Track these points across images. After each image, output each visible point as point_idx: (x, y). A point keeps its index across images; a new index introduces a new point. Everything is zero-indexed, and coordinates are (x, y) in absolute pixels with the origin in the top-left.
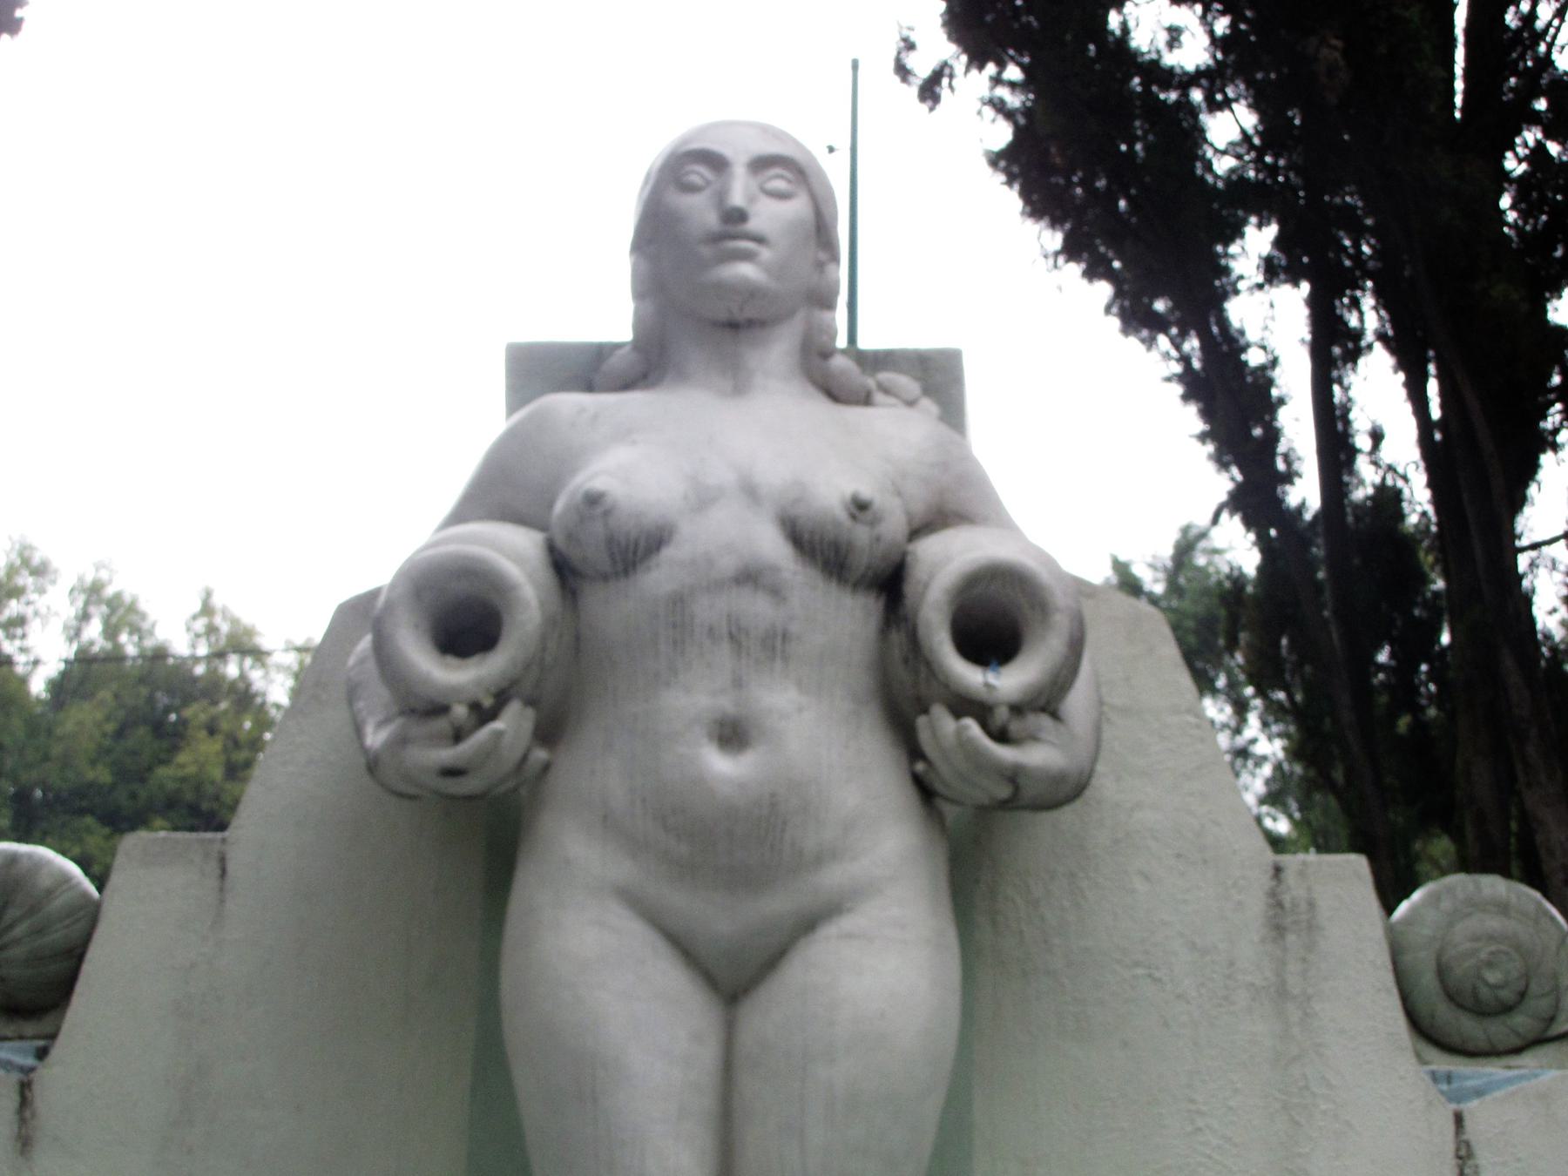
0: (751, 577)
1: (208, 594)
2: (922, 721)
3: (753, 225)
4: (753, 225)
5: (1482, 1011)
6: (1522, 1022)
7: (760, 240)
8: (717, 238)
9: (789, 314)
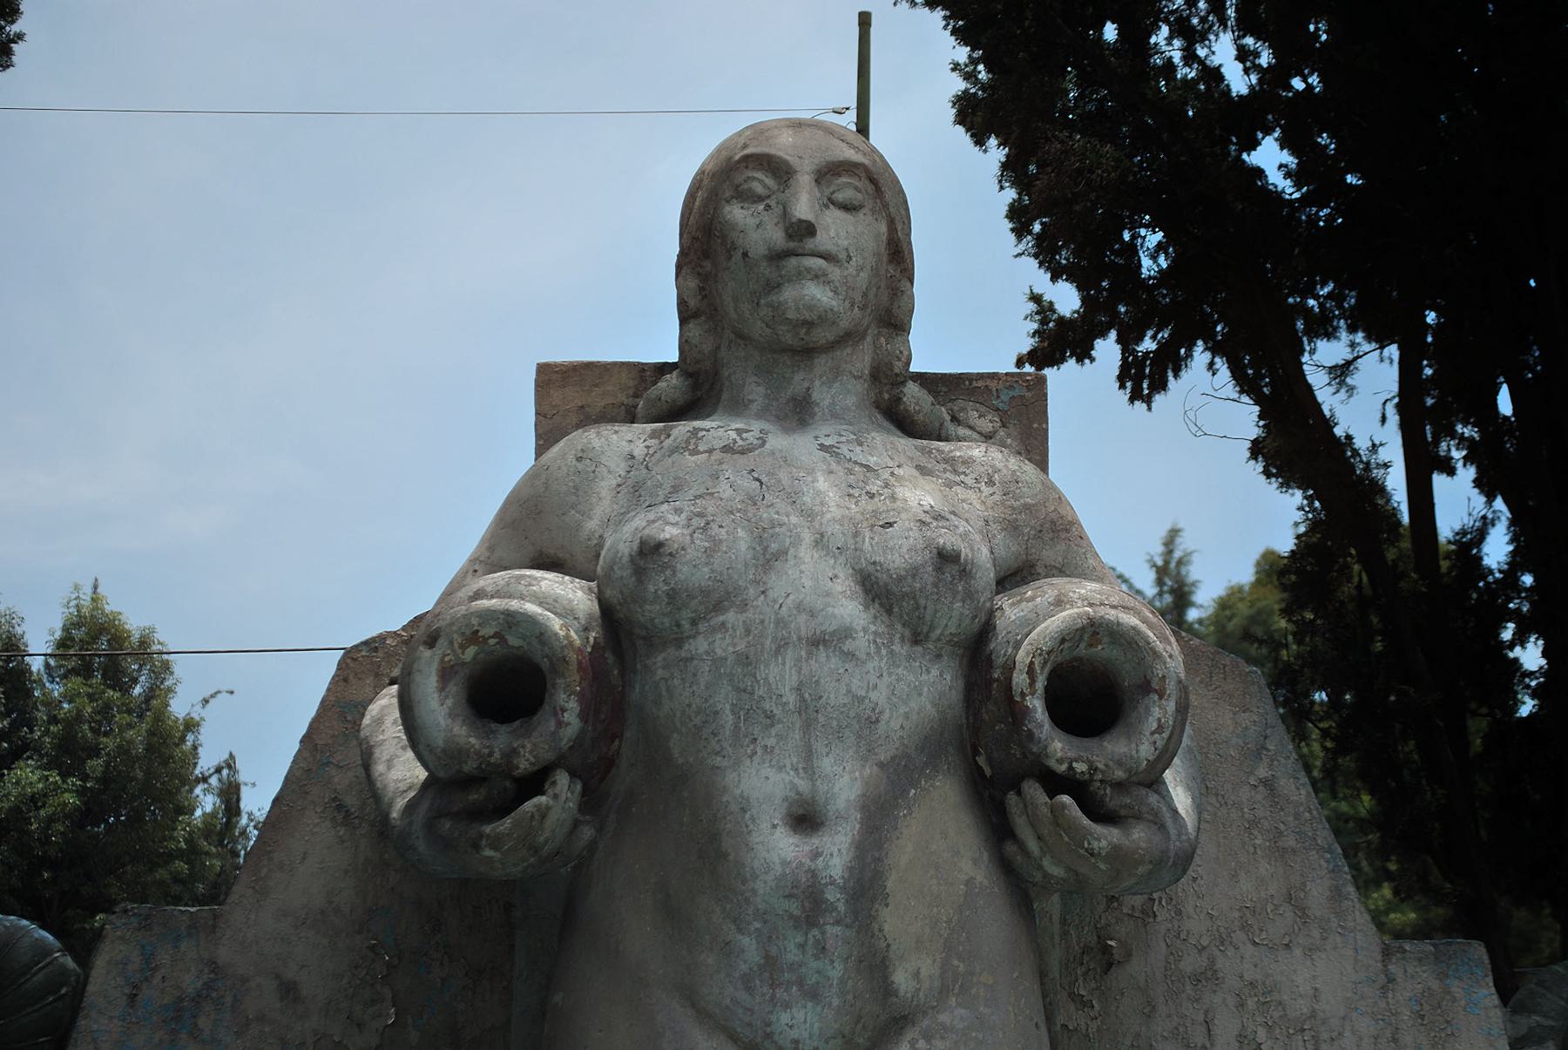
0: (880, 604)
1: (1150, 409)
2: (1012, 798)
3: (822, 240)
4: (822, 240)
7: (827, 256)
8: (777, 256)
9: (849, 338)
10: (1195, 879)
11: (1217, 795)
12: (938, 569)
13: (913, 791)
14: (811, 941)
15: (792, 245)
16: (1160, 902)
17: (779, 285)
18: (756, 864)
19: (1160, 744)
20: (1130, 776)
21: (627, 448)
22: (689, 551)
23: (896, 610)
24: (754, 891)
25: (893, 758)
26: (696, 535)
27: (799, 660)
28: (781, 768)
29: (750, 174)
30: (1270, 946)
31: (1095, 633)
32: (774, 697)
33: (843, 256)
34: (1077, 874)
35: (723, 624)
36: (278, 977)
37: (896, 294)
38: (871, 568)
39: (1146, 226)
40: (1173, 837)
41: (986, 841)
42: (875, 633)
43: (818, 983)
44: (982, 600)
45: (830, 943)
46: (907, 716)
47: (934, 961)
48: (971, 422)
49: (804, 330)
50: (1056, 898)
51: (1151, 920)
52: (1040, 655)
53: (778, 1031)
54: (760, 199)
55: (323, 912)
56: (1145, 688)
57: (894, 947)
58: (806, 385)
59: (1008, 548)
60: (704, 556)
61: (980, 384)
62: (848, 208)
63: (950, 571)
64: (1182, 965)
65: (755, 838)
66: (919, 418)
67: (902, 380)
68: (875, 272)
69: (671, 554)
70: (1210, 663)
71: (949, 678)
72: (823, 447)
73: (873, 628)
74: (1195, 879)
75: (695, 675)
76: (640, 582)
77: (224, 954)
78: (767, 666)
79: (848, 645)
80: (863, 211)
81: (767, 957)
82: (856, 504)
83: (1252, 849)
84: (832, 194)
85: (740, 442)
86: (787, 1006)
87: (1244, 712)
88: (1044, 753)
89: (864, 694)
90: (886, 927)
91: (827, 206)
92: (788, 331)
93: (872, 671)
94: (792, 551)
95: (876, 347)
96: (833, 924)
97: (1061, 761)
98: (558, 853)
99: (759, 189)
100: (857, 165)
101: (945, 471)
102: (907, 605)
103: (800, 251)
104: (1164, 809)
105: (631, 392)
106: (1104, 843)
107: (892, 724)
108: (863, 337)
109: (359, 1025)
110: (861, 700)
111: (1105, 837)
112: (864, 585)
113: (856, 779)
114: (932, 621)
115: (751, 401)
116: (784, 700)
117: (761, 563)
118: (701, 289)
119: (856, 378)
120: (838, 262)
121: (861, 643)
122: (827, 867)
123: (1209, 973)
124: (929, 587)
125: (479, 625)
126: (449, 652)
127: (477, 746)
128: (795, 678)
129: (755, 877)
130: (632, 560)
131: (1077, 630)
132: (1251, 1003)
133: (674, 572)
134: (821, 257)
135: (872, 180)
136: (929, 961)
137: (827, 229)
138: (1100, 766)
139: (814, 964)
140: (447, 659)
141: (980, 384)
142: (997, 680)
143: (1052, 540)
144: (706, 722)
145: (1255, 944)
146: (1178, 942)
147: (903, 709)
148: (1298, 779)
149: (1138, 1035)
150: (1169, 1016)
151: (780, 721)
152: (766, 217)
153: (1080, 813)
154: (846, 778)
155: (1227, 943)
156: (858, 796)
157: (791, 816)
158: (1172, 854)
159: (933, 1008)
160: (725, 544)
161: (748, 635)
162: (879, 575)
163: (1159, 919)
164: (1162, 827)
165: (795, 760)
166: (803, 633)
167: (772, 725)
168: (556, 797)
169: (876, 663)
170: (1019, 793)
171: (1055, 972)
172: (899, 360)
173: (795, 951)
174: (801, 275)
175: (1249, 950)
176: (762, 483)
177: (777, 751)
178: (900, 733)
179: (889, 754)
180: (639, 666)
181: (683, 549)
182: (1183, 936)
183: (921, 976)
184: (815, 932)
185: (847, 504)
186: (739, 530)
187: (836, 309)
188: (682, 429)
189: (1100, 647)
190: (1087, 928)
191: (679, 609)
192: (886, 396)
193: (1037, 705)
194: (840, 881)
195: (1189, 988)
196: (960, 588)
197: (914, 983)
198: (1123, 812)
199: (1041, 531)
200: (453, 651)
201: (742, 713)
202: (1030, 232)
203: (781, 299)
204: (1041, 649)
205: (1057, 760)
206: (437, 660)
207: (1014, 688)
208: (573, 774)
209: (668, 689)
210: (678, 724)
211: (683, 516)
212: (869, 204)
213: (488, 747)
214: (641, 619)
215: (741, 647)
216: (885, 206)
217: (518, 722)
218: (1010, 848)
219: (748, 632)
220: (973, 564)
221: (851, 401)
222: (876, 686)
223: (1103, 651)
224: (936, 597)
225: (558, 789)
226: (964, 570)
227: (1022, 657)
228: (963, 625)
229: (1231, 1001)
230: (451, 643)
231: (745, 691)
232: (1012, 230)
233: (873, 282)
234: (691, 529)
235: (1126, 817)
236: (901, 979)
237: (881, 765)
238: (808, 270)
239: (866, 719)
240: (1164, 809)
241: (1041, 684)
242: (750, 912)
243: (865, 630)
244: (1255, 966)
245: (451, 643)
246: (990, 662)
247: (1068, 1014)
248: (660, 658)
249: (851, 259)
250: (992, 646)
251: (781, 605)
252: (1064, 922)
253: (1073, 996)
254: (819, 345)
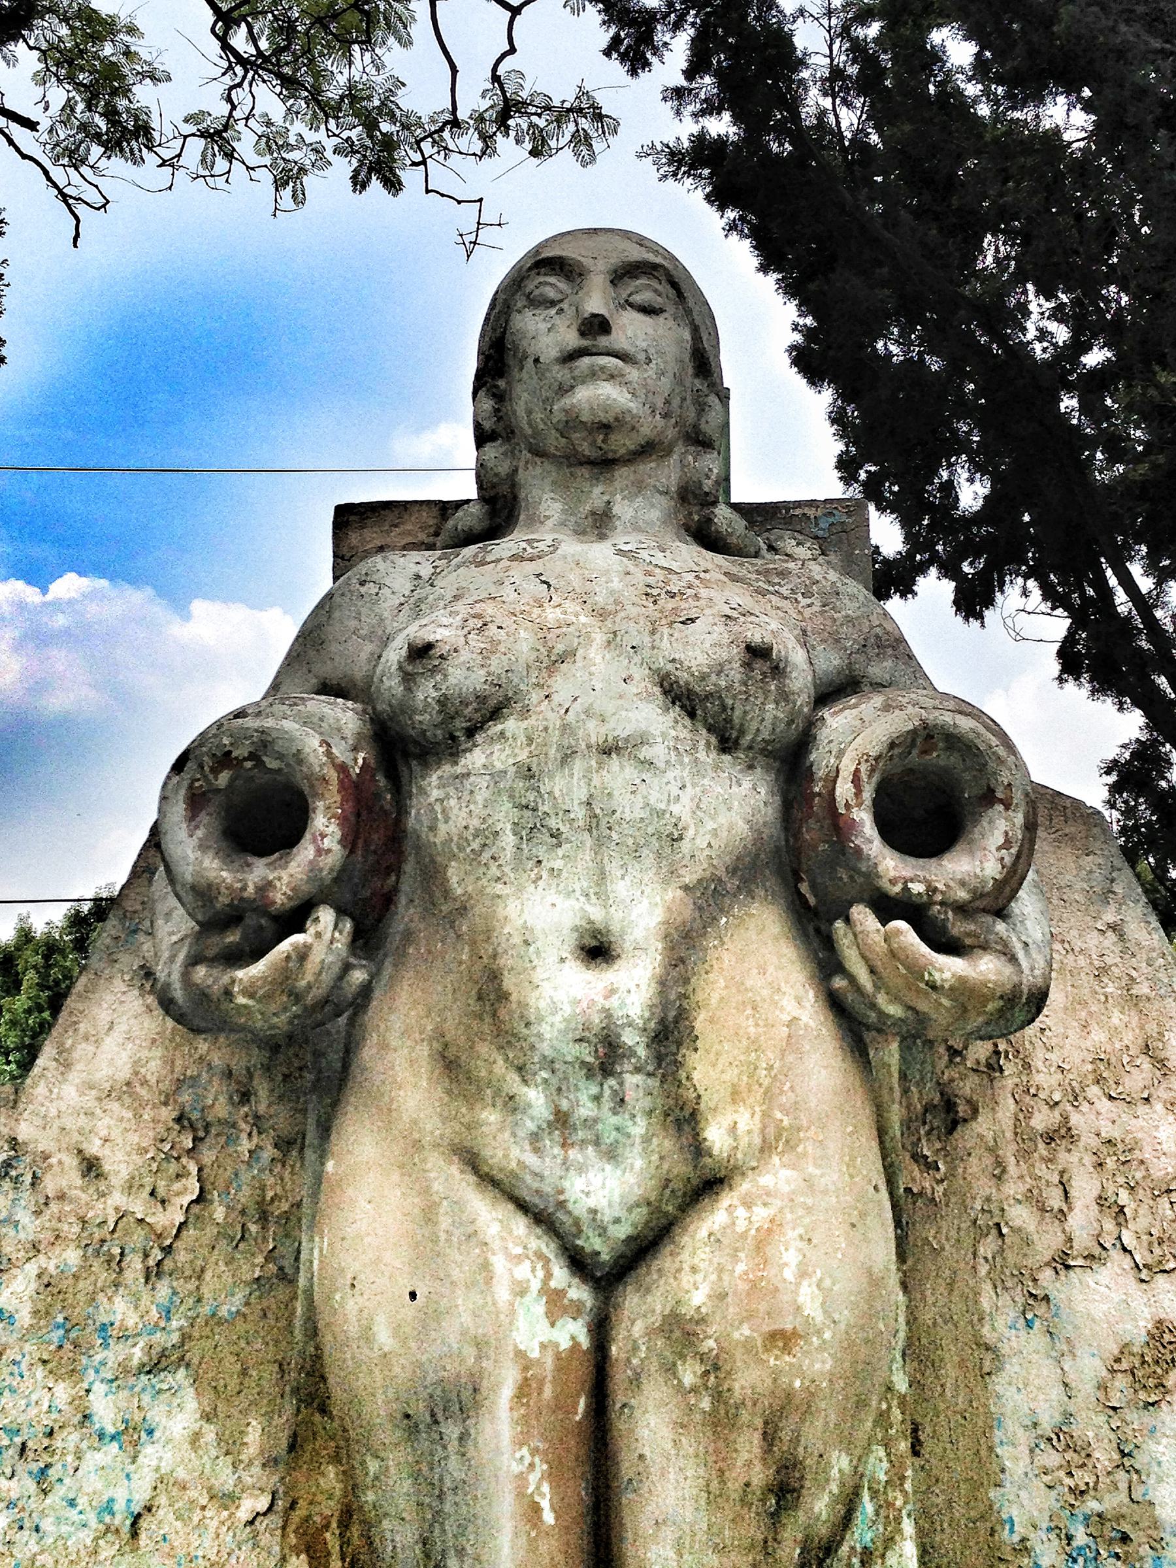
0: (682, 707)
7: (623, 357)
10: (1042, 1030)
11: (1063, 942)
12: (747, 665)
13: (724, 920)
14: (607, 1092)
15: (585, 343)
16: (1007, 1057)
17: (572, 387)
18: (542, 1004)
19: (1008, 860)
20: (974, 899)
21: (415, 569)
22: (462, 652)
23: (699, 712)
24: (539, 1036)
25: (700, 881)
26: (470, 636)
27: (589, 770)
28: (570, 893)
29: (542, 279)
30: (1128, 1100)
31: (930, 737)
32: (561, 813)
33: (641, 357)
34: (917, 1012)
35: (502, 733)
36: (80, 1152)
37: (703, 410)
38: (670, 667)
40: (1027, 971)
41: (794, 938)
42: (677, 738)
43: (617, 1142)
44: (799, 703)
45: (630, 1096)
46: (715, 833)
47: (753, 1115)
48: (789, 551)
49: (601, 437)
50: (894, 1046)
51: (997, 1074)
52: (867, 761)
53: (572, 1200)
54: (553, 303)
55: (128, 1084)
57: (704, 1099)
58: (606, 498)
59: (830, 661)
60: (480, 657)
61: (797, 512)
62: (648, 310)
63: (759, 666)
64: (1033, 1123)
65: (538, 975)
66: (733, 540)
67: (713, 499)
68: (678, 380)
69: (441, 657)
70: (1049, 806)
71: (763, 792)
72: (620, 552)
73: (673, 733)
74: (1042, 1030)
75: (472, 792)
76: (409, 689)
77: (24, 1131)
78: (551, 777)
79: (645, 753)
80: (665, 315)
82: (655, 603)
83: (1103, 998)
84: (629, 296)
85: (529, 550)
86: (581, 1169)
87: (1087, 855)
88: (872, 875)
89: (663, 806)
90: (696, 1076)
91: (623, 307)
92: (584, 439)
93: (673, 782)
94: (580, 653)
95: (683, 465)
96: (632, 1073)
97: (893, 882)
98: (327, 1002)
99: (551, 293)
100: (656, 267)
101: (757, 580)
102: (712, 707)
103: (594, 350)
104: (1014, 939)
105: (432, 530)
106: (947, 975)
107: (698, 841)
108: (669, 453)
109: (163, 1202)
110: (660, 814)
111: (948, 968)
112: (662, 686)
113: (656, 904)
114: (742, 725)
115: (547, 517)
116: (572, 816)
117: (544, 665)
118: (497, 410)
119: (661, 493)
120: (636, 363)
121: (657, 752)
122: (623, 1004)
123: (1063, 1131)
124: (736, 685)
125: (232, 744)
126: (198, 776)
127: (228, 881)
128: (585, 791)
129: (541, 1019)
130: (400, 668)
131: (908, 732)
132: (1110, 1163)
133: (446, 676)
134: (616, 356)
135: (674, 285)
136: (747, 1115)
137: (623, 328)
138: (941, 886)
139: (614, 1120)
140: (197, 784)
141: (797, 512)
142: (819, 794)
143: (878, 655)
144: (485, 845)
145: (1111, 1098)
146: (1028, 1098)
147: (710, 825)
148: (1149, 923)
149: (988, 1199)
150: (1021, 1177)
151: (568, 841)
152: (557, 320)
153: (918, 940)
154: (646, 902)
155: (1080, 1099)
156: (659, 923)
157: (582, 949)
158: (1026, 991)
159: (753, 1169)
160: (503, 645)
161: (529, 745)
162: (678, 673)
163: (1006, 1073)
164: (1013, 959)
165: (585, 884)
166: (593, 740)
167: (559, 845)
168: (318, 935)
169: (677, 772)
170: (847, 920)
171: (896, 1129)
172: (708, 478)
173: (590, 1105)
174: (594, 375)
175: (1104, 1105)
176: (549, 586)
177: (565, 874)
178: (707, 852)
179: (695, 877)
180: (414, 790)
181: (456, 651)
182: (1032, 1091)
183: (739, 1132)
184: (612, 1082)
185: (645, 603)
186: (522, 631)
187: (635, 411)
189: (935, 754)
190: (929, 1085)
191: (452, 718)
192: (696, 518)
193: (864, 818)
194: (640, 1023)
195: (1041, 1146)
196: (773, 687)
197: (731, 1141)
198: (968, 941)
199: (864, 646)
200: (205, 777)
201: (524, 833)
202: (857, 481)
203: (575, 401)
204: (867, 754)
205: (890, 881)
206: (186, 784)
207: (838, 799)
208: (341, 912)
209: (443, 811)
210: (456, 850)
211: (458, 618)
212: (671, 309)
213: (241, 881)
214: (412, 733)
215: (523, 756)
216: (688, 312)
217: (277, 855)
218: (839, 983)
219: (530, 740)
220: (787, 661)
221: (655, 514)
222: (678, 798)
223: (938, 758)
224: (744, 697)
225: (320, 927)
226: (777, 667)
227: (847, 766)
228: (778, 730)
229: (1089, 1160)
230: (201, 766)
231: (527, 807)
232: (841, 478)
233: (677, 391)
234: (466, 630)
235: (972, 947)
236: (716, 1136)
237: (686, 888)
238: (603, 369)
239: (667, 836)
240: (1014, 939)
241: (868, 794)
242: (536, 1060)
243: (664, 735)
244: (1114, 1122)
245: (201, 766)
246: (809, 775)
247: (912, 1176)
248: (435, 777)
249: (650, 361)
250: (813, 757)
251: (567, 711)
252: (903, 1077)
253: (917, 1157)
254: (618, 455)
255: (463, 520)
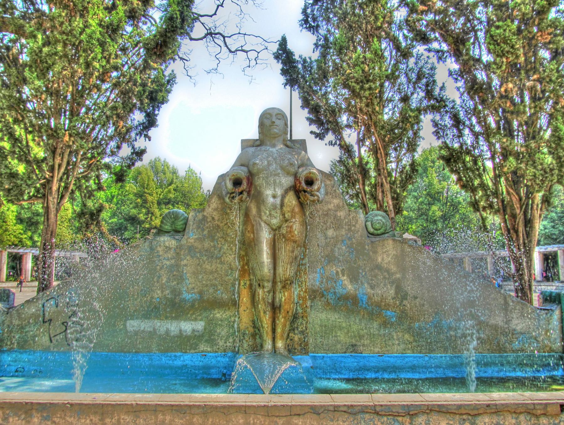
4: (276, 124)
5: (377, 230)
6: (382, 231)
8: (270, 126)
39: (12, 14)
56: (317, 180)
81: (393, 73)
188: (259, 148)
255: (258, 143)
